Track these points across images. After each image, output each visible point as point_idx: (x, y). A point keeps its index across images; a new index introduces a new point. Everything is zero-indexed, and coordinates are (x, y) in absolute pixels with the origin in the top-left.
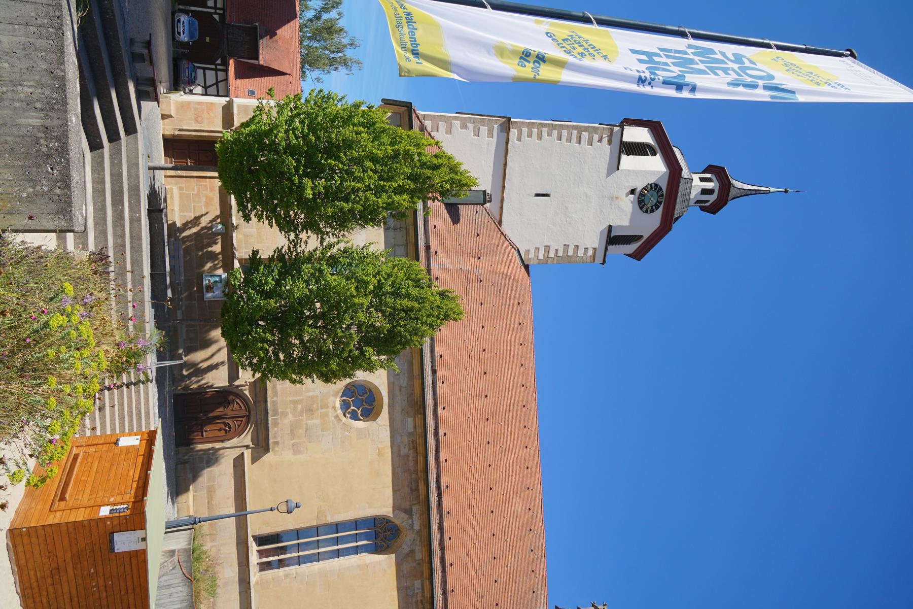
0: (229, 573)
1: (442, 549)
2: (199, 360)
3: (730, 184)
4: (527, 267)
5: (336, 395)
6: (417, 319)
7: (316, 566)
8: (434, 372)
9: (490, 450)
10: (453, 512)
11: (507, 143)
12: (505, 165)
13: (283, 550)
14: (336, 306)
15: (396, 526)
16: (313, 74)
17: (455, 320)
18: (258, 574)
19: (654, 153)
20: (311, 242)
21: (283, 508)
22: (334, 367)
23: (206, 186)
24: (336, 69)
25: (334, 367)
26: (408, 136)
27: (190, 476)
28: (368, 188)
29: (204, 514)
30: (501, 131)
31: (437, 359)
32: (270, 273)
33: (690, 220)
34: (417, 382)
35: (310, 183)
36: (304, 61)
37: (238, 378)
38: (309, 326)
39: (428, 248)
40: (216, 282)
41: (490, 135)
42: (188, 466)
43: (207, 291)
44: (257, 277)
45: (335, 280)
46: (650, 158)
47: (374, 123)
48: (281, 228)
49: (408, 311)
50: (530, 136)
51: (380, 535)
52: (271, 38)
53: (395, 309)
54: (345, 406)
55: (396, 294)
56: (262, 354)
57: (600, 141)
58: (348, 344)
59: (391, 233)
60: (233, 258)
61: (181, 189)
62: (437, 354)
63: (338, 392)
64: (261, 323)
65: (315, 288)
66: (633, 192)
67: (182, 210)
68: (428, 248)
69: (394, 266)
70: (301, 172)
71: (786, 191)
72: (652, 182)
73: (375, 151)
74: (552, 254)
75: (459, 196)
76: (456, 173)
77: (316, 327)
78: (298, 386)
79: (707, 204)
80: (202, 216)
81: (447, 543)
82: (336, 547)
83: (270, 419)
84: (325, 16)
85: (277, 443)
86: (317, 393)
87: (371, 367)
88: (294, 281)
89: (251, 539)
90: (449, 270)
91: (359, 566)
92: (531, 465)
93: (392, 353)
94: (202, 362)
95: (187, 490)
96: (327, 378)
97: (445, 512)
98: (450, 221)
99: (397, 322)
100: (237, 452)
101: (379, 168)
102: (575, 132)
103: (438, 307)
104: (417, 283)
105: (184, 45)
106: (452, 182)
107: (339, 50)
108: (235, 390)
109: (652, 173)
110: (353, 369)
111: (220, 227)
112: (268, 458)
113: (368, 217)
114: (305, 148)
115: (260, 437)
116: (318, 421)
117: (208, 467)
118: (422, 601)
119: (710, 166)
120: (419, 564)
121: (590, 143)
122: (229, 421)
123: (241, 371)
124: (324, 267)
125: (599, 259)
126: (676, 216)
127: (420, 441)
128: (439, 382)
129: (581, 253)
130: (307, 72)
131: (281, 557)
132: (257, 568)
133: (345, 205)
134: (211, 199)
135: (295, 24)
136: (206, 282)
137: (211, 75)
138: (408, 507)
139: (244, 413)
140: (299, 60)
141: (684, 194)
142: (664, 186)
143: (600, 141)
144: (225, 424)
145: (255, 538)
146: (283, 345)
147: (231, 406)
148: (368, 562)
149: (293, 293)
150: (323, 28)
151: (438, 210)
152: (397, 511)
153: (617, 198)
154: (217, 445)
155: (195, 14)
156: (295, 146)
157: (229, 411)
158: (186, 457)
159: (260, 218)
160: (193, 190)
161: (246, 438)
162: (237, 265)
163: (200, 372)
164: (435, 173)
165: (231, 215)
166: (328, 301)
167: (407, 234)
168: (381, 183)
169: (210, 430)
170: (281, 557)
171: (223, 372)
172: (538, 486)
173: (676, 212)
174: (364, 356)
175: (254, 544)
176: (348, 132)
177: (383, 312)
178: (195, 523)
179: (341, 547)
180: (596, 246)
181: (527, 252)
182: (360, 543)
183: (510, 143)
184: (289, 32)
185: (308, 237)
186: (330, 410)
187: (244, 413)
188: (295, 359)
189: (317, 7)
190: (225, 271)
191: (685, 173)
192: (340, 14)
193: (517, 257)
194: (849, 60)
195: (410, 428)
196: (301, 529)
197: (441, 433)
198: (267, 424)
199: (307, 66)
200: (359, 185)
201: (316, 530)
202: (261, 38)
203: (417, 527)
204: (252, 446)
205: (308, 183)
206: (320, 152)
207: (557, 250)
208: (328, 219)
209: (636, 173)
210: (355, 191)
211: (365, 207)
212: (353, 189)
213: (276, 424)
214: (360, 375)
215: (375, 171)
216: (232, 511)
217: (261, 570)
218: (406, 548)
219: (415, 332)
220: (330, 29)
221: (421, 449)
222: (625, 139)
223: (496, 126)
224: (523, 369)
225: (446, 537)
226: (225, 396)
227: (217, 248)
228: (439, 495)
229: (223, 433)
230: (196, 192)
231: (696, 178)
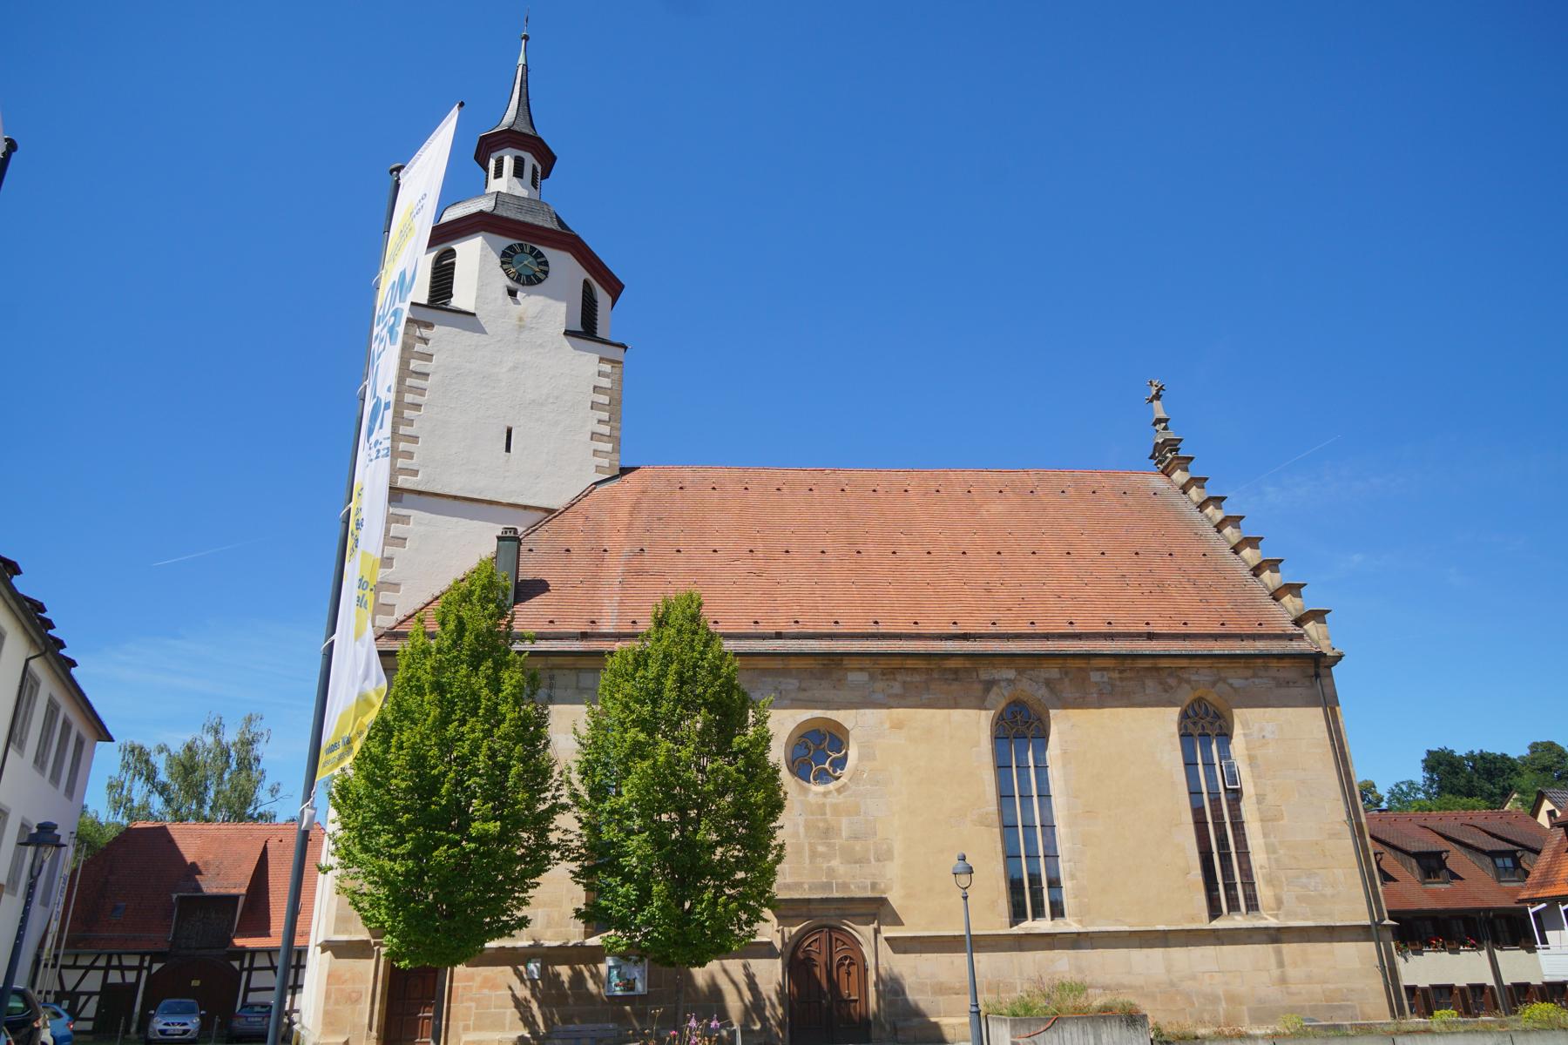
0: (1062, 963)
1: (1047, 637)
2: (739, 1004)
3: (509, 131)
4: (624, 471)
5: (805, 791)
6: (695, 666)
7: (1061, 830)
8: (779, 636)
9: (905, 551)
10: (994, 616)
11: (420, 493)
12: (455, 498)
13: (1035, 879)
14: (668, 789)
15: (1009, 705)
16: (264, 801)
17: (700, 605)
19: (451, 253)
20: (567, 825)
21: (964, 880)
22: (760, 797)
23: (465, 988)
24: (258, 760)
25: (760, 797)
26: (408, 666)
27: (916, 1021)
28: (488, 734)
29: (967, 1000)
31: (760, 629)
32: (613, 890)
33: (563, 198)
34: (794, 664)
35: (476, 824)
36: (240, 817)
37: (770, 943)
38: (696, 831)
39: (584, 636)
40: (619, 975)
41: (404, 520)
43: (633, 989)
44: (616, 910)
45: (629, 791)
46: (458, 260)
47: (383, 720)
48: (539, 871)
49: (682, 681)
50: (410, 455)
51: (1020, 730)
52: (200, 873)
53: (678, 701)
54: (823, 777)
55: (655, 697)
56: (734, 905)
57: (425, 341)
58: (727, 774)
59: (557, 693)
60: (583, 946)
61: (466, 1028)
62: (752, 630)
63: (802, 787)
64: (687, 905)
65: (638, 821)
66: (512, 293)
67: (502, 1027)
68: (584, 636)
69: (612, 697)
70: (458, 837)
71: (526, 38)
73: (430, 720)
74: (605, 429)
75: (507, 588)
76: (471, 593)
77: (699, 822)
78: (788, 849)
79: (539, 169)
80: (514, 996)
81: (1039, 629)
82: (1035, 799)
83: (836, 895)
84: (163, 777)
85: (874, 886)
86: (801, 820)
87: (764, 740)
88: (627, 854)
89: (1016, 930)
90: (621, 603)
91: (1064, 766)
92: (933, 485)
93: (746, 702)
94: (742, 999)
95: (936, 1026)
96: (775, 806)
97: (993, 630)
98: (543, 596)
99: (697, 696)
100: (884, 948)
101: (459, 714)
102: (409, 381)
103: (679, 631)
104: (641, 660)
105: (205, 1024)
106: (485, 600)
107: (225, 753)
108: (790, 948)
109: (483, 258)
110: (765, 767)
111: (532, 966)
112: (895, 899)
113: (532, 733)
114: (421, 829)
115: (863, 911)
116: (844, 821)
117: (904, 993)
118: (1121, 672)
119: (476, 158)
120: (1066, 673)
121: (428, 357)
122: (837, 958)
123: (758, 939)
124: (607, 805)
125: (617, 353)
126: (555, 226)
127: (883, 663)
128: (795, 629)
129: (605, 383)
130: (261, 810)
131: (1045, 884)
132: (1059, 921)
133: (513, 771)
134: (486, 980)
135: (175, 830)
136: (618, 992)
137: (258, 979)
138: (980, 687)
139: (824, 936)
140: (241, 826)
141: (520, 208)
142: (507, 242)
143: (425, 341)
144: (840, 965)
145: (1014, 923)
146: (722, 872)
147: (814, 956)
148: (1058, 752)
149: (646, 856)
150: (185, 780)
151: (528, 617)
153: (521, 319)
154: (872, 977)
155: (151, 1003)
156: (415, 847)
157: (821, 959)
158: (888, 1027)
159: (524, 902)
160: (469, 1008)
162: (595, 941)
163: (756, 1006)
164: (469, 627)
165: (514, 949)
166: (659, 801)
167: (560, 668)
168: (481, 712)
169: (849, 990)
170: (1045, 884)
171: (760, 966)
172: (968, 475)
173: (548, 225)
174: (746, 749)
175: (1022, 925)
176: (398, 761)
177: (682, 718)
178: (978, 1013)
179: (1034, 793)
180: (596, 357)
181: (598, 469)
182: (1031, 763)
183: (420, 488)
184: (191, 841)
185: (557, 828)
186: (829, 800)
187: (824, 936)
188: (746, 856)
189: (145, 790)
190: (602, 960)
191: (485, 204)
192: (161, 749)
193: (606, 486)
194: (405, 177)
195: (864, 677)
196: (1004, 852)
197: (873, 629)
198: (843, 899)
199: (250, 810)
200: (484, 749)
201: (1008, 827)
202: (199, 889)
203: (1011, 674)
204: (875, 925)
205: (476, 827)
206: (428, 805)
207: (600, 421)
208: (534, 798)
209: (482, 285)
210: (493, 755)
211: (519, 739)
212: (490, 758)
213: (845, 886)
214: (777, 754)
215: (463, 722)
216: (964, 957)
217: (1062, 915)
218: (1042, 692)
219: (715, 671)
220: (187, 767)
221: (896, 663)
222: (425, 302)
224: (785, 490)
225: (1029, 630)
226: (797, 963)
227: (564, 972)
228: (965, 637)
229: (853, 969)
230: (473, 1004)
231: (496, 185)
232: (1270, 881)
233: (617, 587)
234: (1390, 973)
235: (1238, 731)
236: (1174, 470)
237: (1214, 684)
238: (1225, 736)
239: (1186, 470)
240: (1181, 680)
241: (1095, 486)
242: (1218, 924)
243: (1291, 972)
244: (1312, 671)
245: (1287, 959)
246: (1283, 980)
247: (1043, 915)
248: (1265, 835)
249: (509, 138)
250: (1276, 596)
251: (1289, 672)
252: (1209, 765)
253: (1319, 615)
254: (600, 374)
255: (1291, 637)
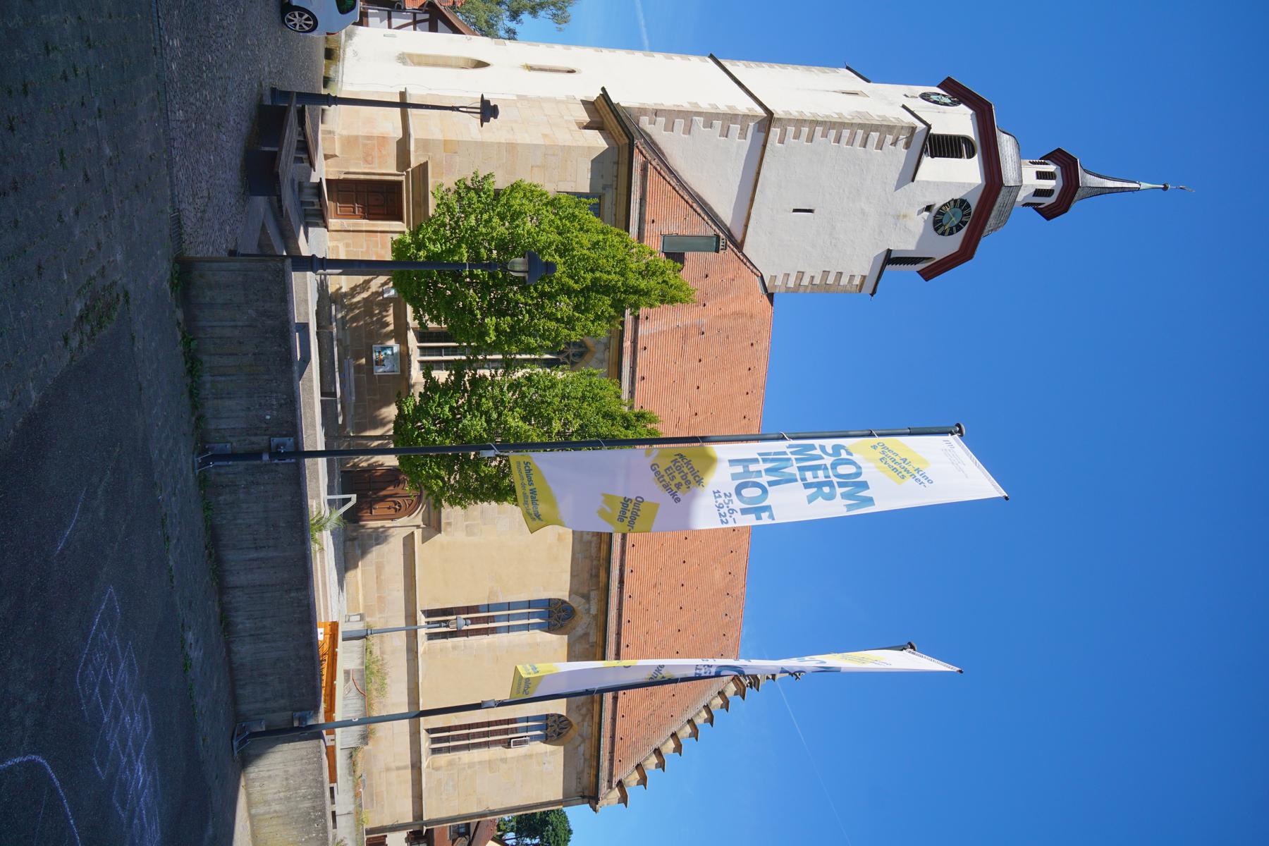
1: (619, 634)
4: (771, 297)
10: (636, 595)
11: (764, 146)
12: (758, 173)
18: (427, 643)
27: (359, 552)
30: (759, 130)
41: (743, 135)
42: (356, 543)
46: (964, 161)
50: (797, 136)
57: (894, 143)
61: (347, 245)
66: (928, 208)
71: (1165, 188)
72: (957, 197)
74: (806, 282)
85: (449, 524)
90: (662, 332)
95: (356, 566)
100: (407, 531)
109: (962, 185)
111: (393, 292)
112: (438, 537)
122: (399, 500)
125: (868, 288)
129: (844, 281)
136: (375, 355)
138: (585, 591)
141: (1005, 205)
143: (894, 143)
144: (395, 503)
145: (424, 612)
152: (576, 594)
153: (905, 216)
154: (388, 523)
157: (398, 490)
161: (417, 518)
169: (379, 508)
180: (866, 273)
181: (774, 278)
190: (397, 342)
203: (593, 611)
207: (813, 277)
218: (579, 631)
223: (752, 124)
224: (744, 422)
232: (451, 763)
233: (673, 325)
234: (395, 828)
235: (548, 748)
236: (736, 685)
237: (581, 736)
238: (546, 739)
239: (736, 694)
240: (584, 716)
241: (729, 635)
242: (423, 734)
243: (393, 774)
244: (586, 793)
245: (401, 772)
246: (388, 769)
247: (422, 355)
248: (480, 762)
249: (1071, 187)
250: (639, 767)
251: (587, 779)
252: (527, 729)
253: (624, 799)
254: (852, 277)
255: (610, 781)
